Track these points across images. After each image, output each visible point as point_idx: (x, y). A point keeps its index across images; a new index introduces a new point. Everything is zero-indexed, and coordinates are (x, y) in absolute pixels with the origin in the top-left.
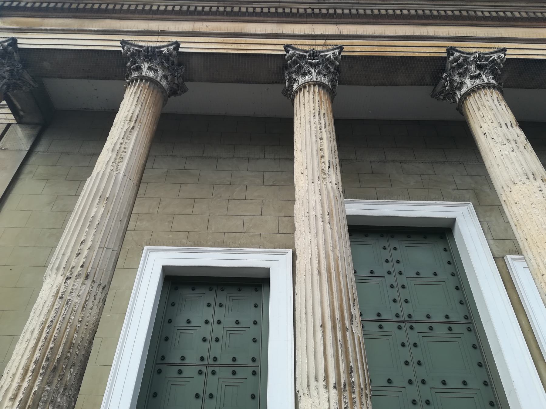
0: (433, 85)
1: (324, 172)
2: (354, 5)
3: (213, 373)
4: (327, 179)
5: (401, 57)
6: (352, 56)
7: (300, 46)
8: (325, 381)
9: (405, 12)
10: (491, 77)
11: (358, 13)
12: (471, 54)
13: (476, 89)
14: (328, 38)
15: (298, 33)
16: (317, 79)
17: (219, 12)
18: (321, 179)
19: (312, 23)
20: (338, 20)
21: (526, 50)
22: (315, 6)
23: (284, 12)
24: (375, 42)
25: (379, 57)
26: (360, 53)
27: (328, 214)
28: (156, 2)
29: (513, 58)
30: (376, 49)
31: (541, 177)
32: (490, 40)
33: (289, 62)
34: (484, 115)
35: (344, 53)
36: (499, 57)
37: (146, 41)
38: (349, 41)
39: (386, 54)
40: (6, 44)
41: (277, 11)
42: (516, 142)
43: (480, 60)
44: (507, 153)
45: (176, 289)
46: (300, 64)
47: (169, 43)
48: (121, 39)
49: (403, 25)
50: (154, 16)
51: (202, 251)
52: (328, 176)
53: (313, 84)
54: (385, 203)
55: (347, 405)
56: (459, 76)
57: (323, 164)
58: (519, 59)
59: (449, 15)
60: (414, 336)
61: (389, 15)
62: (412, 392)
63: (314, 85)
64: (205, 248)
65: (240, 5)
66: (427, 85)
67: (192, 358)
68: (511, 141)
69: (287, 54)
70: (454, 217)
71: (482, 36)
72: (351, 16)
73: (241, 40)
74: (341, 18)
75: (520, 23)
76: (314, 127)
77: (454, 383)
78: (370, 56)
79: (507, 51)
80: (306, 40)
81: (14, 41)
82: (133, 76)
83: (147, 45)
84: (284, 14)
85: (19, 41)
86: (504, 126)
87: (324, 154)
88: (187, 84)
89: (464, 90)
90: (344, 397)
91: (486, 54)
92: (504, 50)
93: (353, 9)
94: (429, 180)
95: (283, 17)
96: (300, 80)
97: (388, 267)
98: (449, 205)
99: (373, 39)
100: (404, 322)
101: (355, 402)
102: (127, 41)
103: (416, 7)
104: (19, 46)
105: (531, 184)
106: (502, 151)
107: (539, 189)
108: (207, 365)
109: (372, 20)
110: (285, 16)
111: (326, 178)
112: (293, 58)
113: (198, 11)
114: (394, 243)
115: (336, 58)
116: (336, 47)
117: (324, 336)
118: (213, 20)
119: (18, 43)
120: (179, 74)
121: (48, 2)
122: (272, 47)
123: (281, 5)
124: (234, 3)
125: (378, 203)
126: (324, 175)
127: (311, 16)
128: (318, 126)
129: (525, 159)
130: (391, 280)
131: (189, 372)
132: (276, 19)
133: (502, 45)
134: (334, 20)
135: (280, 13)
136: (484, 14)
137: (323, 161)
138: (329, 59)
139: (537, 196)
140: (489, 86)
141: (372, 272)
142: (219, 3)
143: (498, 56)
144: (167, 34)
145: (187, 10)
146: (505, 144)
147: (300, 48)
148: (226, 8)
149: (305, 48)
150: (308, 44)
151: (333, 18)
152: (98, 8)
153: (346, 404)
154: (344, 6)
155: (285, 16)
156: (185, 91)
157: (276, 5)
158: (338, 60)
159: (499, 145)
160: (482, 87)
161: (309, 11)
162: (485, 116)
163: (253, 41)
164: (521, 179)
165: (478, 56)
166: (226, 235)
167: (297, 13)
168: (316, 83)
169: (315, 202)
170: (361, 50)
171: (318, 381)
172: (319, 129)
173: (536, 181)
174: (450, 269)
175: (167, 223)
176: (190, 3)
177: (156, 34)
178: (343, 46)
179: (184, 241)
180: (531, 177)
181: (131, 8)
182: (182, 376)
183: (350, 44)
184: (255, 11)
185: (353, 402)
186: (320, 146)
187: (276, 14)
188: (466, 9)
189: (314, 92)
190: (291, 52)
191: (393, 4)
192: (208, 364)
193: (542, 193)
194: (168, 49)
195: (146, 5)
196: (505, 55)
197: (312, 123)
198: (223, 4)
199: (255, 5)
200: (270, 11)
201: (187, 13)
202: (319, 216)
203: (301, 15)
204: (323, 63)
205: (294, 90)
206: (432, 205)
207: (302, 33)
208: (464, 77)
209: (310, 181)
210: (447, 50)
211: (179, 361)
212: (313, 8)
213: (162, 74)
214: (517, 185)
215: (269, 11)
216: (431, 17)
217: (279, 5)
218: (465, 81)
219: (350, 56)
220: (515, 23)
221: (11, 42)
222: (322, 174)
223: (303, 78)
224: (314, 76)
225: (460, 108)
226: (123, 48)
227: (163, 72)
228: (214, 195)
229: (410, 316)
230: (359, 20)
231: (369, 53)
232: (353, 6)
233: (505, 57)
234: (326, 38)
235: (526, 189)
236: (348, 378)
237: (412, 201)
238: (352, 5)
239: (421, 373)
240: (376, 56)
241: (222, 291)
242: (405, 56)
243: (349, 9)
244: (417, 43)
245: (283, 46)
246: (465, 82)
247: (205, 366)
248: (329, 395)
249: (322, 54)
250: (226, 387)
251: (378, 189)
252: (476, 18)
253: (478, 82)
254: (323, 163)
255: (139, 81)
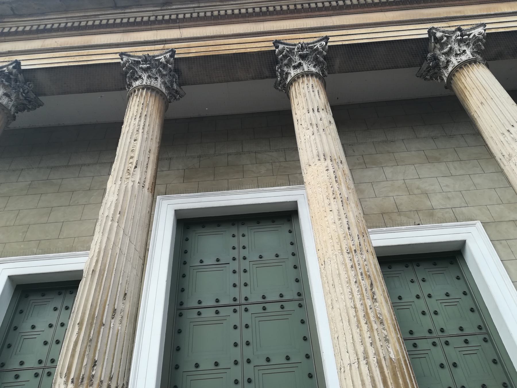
2: (195, 9)
3: (196, 366)
9: (243, 11)
12: (295, 45)
13: (296, 79)
15: (285, 28)
16: (146, 83)
17: (179, 19)
18: (124, 179)
20: (180, 24)
21: (352, 36)
22: (158, 13)
23: (191, 17)
25: (213, 56)
27: (119, 213)
28: (8, 25)
30: (211, 49)
33: (124, 69)
35: (180, 55)
36: (321, 45)
37: (466, 25)
38: (183, 44)
39: (220, 52)
40: (11, 67)
42: (317, 126)
43: (302, 50)
45: (27, 296)
46: (290, 57)
48: (120, 52)
49: (499, 3)
51: (47, 258)
52: (133, 176)
54: (233, 193)
56: (287, 67)
57: (130, 165)
60: (247, 318)
62: (236, 372)
63: (143, 89)
64: (51, 255)
66: (267, 77)
67: (31, 362)
69: (277, 50)
70: (295, 200)
71: (312, 26)
73: (84, 52)
74: (351, 9)
75: (352, 11)
77: (278, 359)
78: (205, 56)
81: (18, 64)
82: (134, 86)
85: (23, 63)
86: (311, 111)
89: (450, 69)
91: (311, 43)
92: (326, 38)
93: (194, 13)
96: (292, 72)
97: (235, 253)
99: (210, 39)
100: (240, 305)
102: (125, 53)
104: (23, 68)
105: (321, 165)
107: (326, 169)
109: (213, 22)
110: (144, 24)
111: (129, 178)
112: (127, 65)
113: (152, 21)
114: (243, 230)
116: (168, 50)
117: (79, 334)
118: (492, 2)
119: (22, 65)
122: (112, 56)
124: (81, 18)
126: (128, 175)
128: (137, 127)
129: (321, 141)
130: (234, 265)
132: (122, 29)
133: (324, 34)
134: (177, 25)
143: (320, 45)
146: (309, 129)
148: (171, 16)
149: (140, 54)
151: (176, 23)
152: (127, 22)
155: (144, 24)
156: (41, 105)
157: (122, 16)
159: (305, 130)
160: (301, 76)
161: (257, 10)
164: (314, 161)
166: (76, 239)
167: (260, 12)
169: (111, 202)
171: (62, 378)
174: (291, 249)
175: (21, 234)
179: (35, 250)
180: (322, 157)
186: (132, 147)
187: (121, 24)
189: (142, 94)
190: (281, 46)
191: (232, 4)
193: (328, 172)
196: (485, 30)
198: (71, 20)
201: (184, 21)
206: (249, 193)
207: (142, 40)
209: (114, 183)
210: (428, 31)
211: (17, 366)
213: (161, 81)
215: (226, 13)
218: (451, 59)
219: (185, 57)
220: (348, 11)
221: (16, 65)
222: (126, 175)
224: (145, 80)
225: (449, 84)
226: (122, 59)
227: (161, 80)
229: (246, 299)
230: (201, 23)
233: (486, 32)
234: (165, 43)
236: (89, 372)
238: (193, 9)
239: (248, 352)
240: (210, 56)
242: (237, 52)
245: (118, 54)
249: (156, 58)
250: (263, 375)
252: (402, 2)
253: (299, 71)
255: (141, 90)
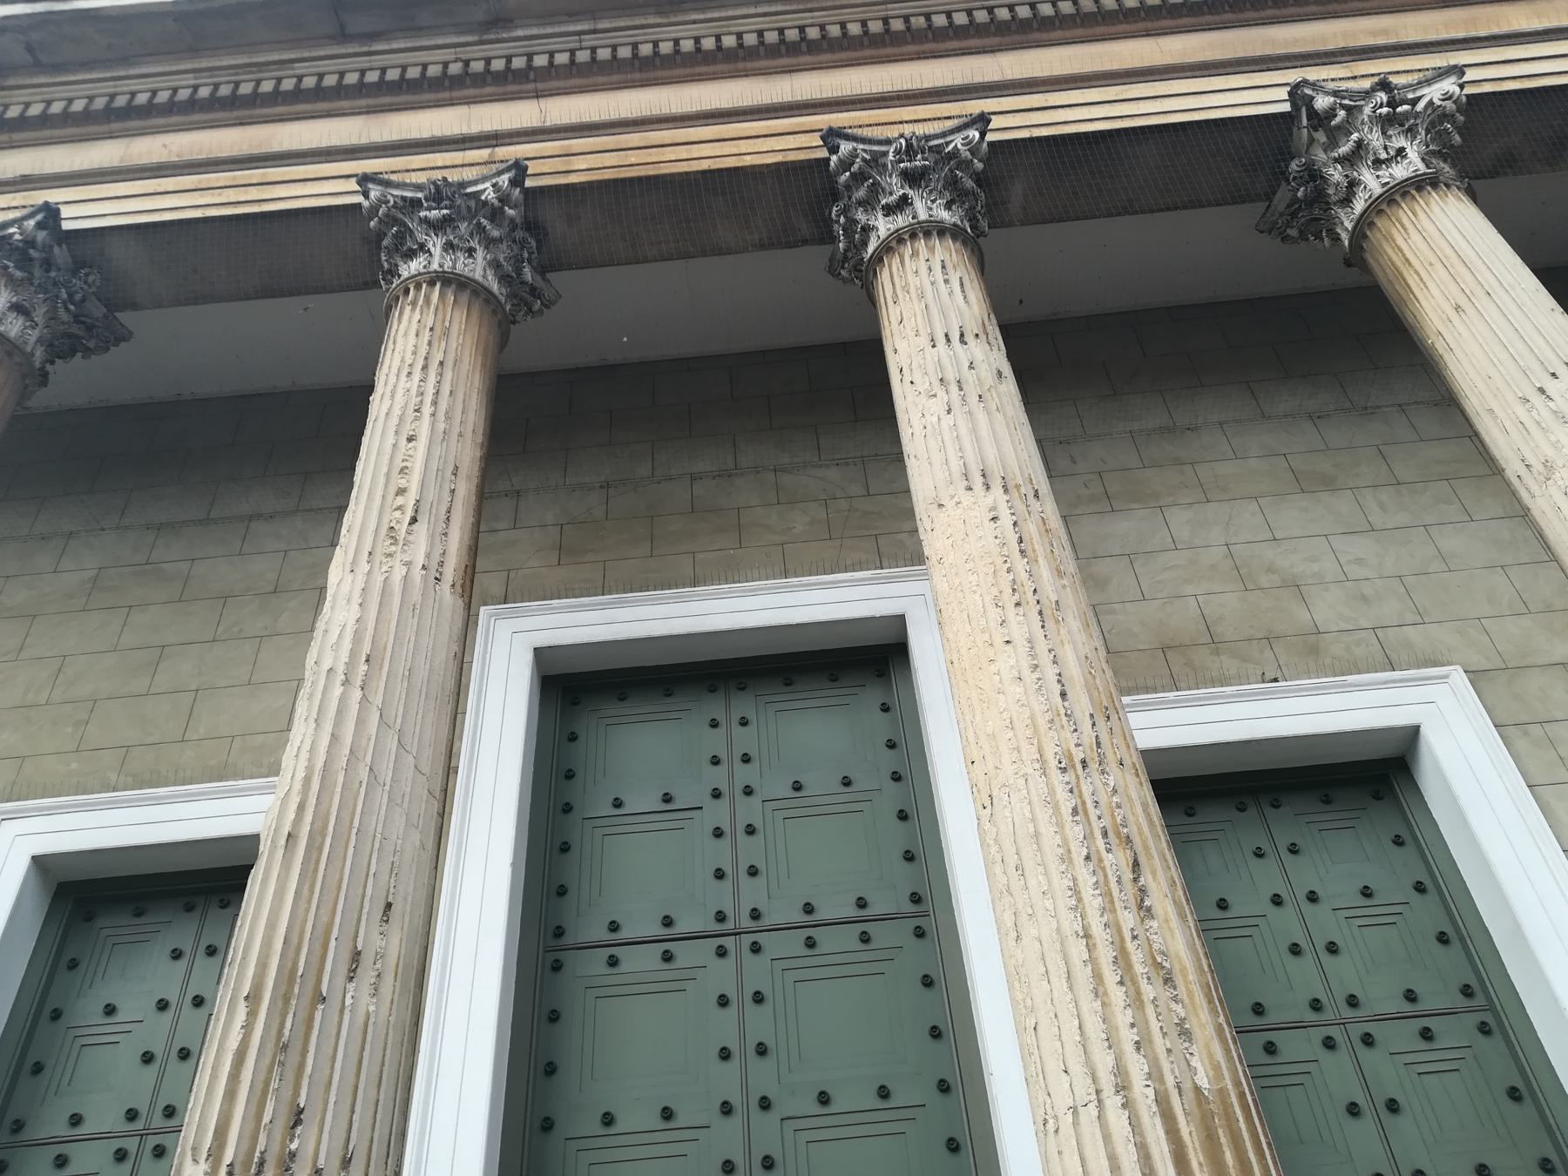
2: (582, 37)
5: (704, 172)
6: (564, 185)
7: (875, 128)
8: (211, 1158)
9: (729, 41)
11: (1035, 15)
12: (888, 142)
14: (500, 142)
17: (831, 40)
19: (468, 103)
20: (540, 86)
22: (473, 52)
26: (585, 175)
27: (367, 661)
28: (16, 96)
30: (633, 157)
31: (1004, 479)
32: (986, 91)
33: (372, 224)
34: (904, 316)
36: (968, 142)
37: (1404, 72)
39: (661, 168)
40: (32, 223)
41: (762, 39)
42: (959, 386)
43: (910, 156)
45: (89, 918)
46: (875, 179)
47: (964, 120)
48: (359, 171)
53: (428, 279)
57: (397, 514)
58: (1039, 139)
59: (1106, 11)
60: (757, 972)
61: (1064, 16)
62: (727, 1139)
63: (432, 283)
66: (805, 242)
69: (834, 158)
70: (899, 612)
72: (1103, 19)
77: (853, 1097)
80: (438, 155)
81: (51, 214)
82: (405, 274)
83: (922, 132)
84: (382, 87)
85: (65, 212)
88: (125, 317)
89: (1359, 205)
91: (936, 136)
92: (982, 120)
93: (581, 49)
94: (846, 513)
95: (781, 56)
97: (718, 778)
98: (889, 580)
100: (735, 934)
102: (374, 176)
103: (760, 23)
104: (66, 226)
105: (974, 503)
106: (928, 416)
109: (637, 76)
111: (395, 552)
114: (744, 704)
117: (248, 1028)
123: (375, 61)
126: (391, 544)
128: (415, 400)
129: (974, 430)
130: (718, 814)
132: (364, 102)
133: (975, 107)
134: (531, 86)
135: (624, 60)
137: (399, 504)
138: (955, 153)
140: (941, 230)
141: (667, 798)
142: (197, 75)
143: (963, 139)
145: (337, 84)
146: (935, 396)
150: (440, 164)
151: (528, 80)
154: (555, 43)
160: (910, 236)
161: (771, 37)
165: (907, 146)
168: (446, 280)
169: (341, 628)
170: (589, 167)
172: (412, 410)
174: (889, 760)
175: (69, 730)
178: (525, 162)
179: (113, 777)
180: (978, 481)
183: (560, 153)
187: (361, 89)
188: (683, 32)
190: (845, 147)
191: (694, 22)
192: (147, 1127)
193: (996, 525)
194: (493, 186)
195: (303, 76)
196: (1462, 86)
197: (400, 392)
202: (341, 669)
209: (348, 568)
210: (1290, 94)
211: (62, 1129)
212: (614, 45)
213: (485, 258)
214: (944, 509)
216: (1226, 6)
217: (370, 61)
218: (1361, 177)
220: (1044, 36)
222: (386, 544)
223: (891, 218)
224: (437, 257)
225: (1358, 253)
226: (366, 194)
227: (487, 254)
229: (755, 915)
230: (601, 79)
235: (961, 519)
238: (577, 38)
239: (764, 1076)
241: (1277, 807)
243: (966, 10)
244: (752, 128)
249: (469, 190)
251: (700, 557)
253: (901, 221)
254: (399, 508)
255: (424, 286)
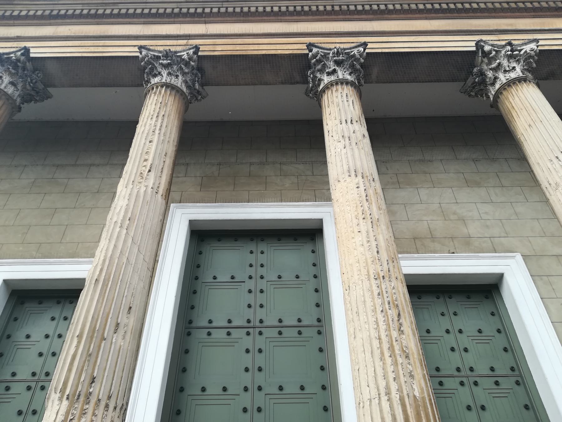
0: (465, 81)
1: (141, 176)
2: (223, 3)
4: (143, 183)
5: (263, 55)
8: (61, 392)
10: (347, 73)
12: (330, 49)
13: (329, 86)
18: (136, 183)
20: (207, 19)
24: (239, 41)
26: (220, 52)
27: (129, 220)
28: (16, 8)
29: (459, 51)
30: (238, 47)
35: (204, 53)
39: (247, 52)
40: (19, 53)
44: (339, 150)
46: (324, 62)
50: (16, 22)
52: (146, 180)
53: (161, 85)
55: (74, 416)
56: (320, 73)
60: (260, 342)
62: (246, 400)
63: (162, 87)
65: (105, 7)
66: (297, 83)
67: (24, 374)
68: (346, 138)
69: (310, 54)
70: (321, 218)
76: (148, 130)
77: (291, 388)
78: (231, 55)
79: (368, 45)
81: (26, 51)
82: (153, 83)
84: (150, 15)
85: (32, 50)
87: (148, 157)
89: (497, 86)
90: (74, 408)
91: (348, 49)
92: (365, 45)
93: (222, 7)
97: (251, 271)
101: (85, 413)
108: (37, 381)
109: (242, 18)
111: (142, 182)
114: (263, 246)
115: (361, 55)
116: (191, 47)
117: (77, 347)
119: (31, 52)
120: (34, 79)
121: (4, 10)
125: (187, 207)
126: (141, 179)
127: (393, 12)
128: (153, 128)
130: (251, 284)
131: (17, 388)
132: (142, 20)
133: (363, 39)
134: (203, 19)
135: (336, 11)
136: (449, 6)
139: (352, 193)
141: (233, 277)
142: (83, 5)
143: (357, 51)
144: (23, 40)
146: (340, 142)
147: (156, 49)
151: (202, 17)
153: (73, 415)
156: (49, 96)
158: (193, 59)
160: (336, 84)
162: (331, 113)
163: (100, 43)
165: (337, 51)
168: (167, 86)
170: (222, 50)
172: (152, 131)
173: (356, 178)
174: (313, 271)
176: (53, 7)
177: (12, 40)
178: (199, 46)
179: (34, 253)
180: (353, 173)
181: (68, 13)
182: (10, 392)
184: (250, 11)
185: (83, 413)
187: (142, 15)
190: (315, 50)
196: (538, 46)
197: (148, 124)
198: (88, 6)
199: (120, 6)
200: (273, 10)
202: (119, 222)
203: (65, 16)
204: (178, 63)
205: (320, 89)
208: (323, 74)
210: (476, 44)
211: (9, 377)
213: (182, 79)
218: (499, 76)
220: (389, 16)
224: (165, 77)
225: (496, 103)
228: (77, 204)
229: (261, 321)
230: (229, 19)
231: (230, 52)
232: (222, 5)
234: (189, 38)
237: (220, 203)
238: (221, 3)
242: (266, 53)
243: (393, 4)
246: (323, 79)
247: (36, 381)
248: (60, 407)
249: (178, 54)
253: (333, 78)
254: (144, 166)
255: (159, 87)
